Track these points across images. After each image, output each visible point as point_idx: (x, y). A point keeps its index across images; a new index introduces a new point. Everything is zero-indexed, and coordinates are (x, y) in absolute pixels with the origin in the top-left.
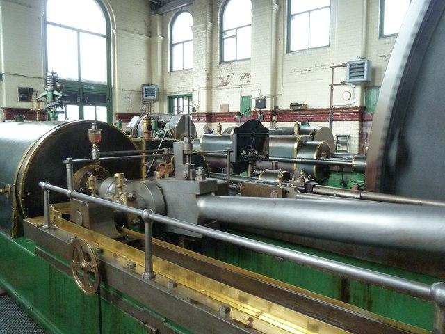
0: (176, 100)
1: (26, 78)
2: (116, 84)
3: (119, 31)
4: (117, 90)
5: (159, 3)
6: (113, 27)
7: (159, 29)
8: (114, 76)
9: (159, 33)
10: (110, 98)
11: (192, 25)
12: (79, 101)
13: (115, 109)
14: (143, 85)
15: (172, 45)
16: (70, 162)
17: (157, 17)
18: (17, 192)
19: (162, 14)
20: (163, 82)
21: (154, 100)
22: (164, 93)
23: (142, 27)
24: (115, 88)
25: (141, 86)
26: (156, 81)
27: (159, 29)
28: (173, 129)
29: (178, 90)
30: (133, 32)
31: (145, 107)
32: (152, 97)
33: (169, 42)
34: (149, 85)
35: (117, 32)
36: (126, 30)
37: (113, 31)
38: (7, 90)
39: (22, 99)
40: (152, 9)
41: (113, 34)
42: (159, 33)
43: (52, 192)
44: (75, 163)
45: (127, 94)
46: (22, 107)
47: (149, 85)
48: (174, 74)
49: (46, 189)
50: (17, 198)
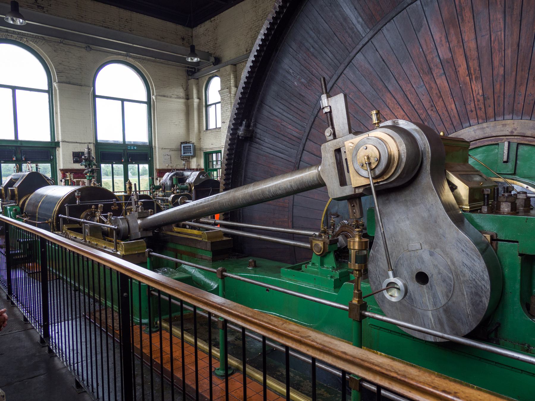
0: (214, 155)
1: (79, 144)
2: (156, 144)
3: (159, 97)
4: (157, 149)
5: (193, 70)
6: (153, 95)
7: (195, 92)
8: (155, 137)
9: (195, 95)
10: (152, 158)
11: (220, 89)
12: (123, 160)
13: (156, 166)
14: (182, 143)
15: (207, 106)
16: (67, 205)
17: (192, 82)
18: (53, 222)
19: (197, 79)
20: (199, 139)
21: (191, 156)
22: (200, 149)
23: (181, 92)
24: (155, 147)
25: (179, 144)
26: (193, 139)
27: (195, 92)
28: (192, 183)
29: (211, 147)
30: (171, 97)
31: (183, 162)
32: (189, 154)
33: (204, 104)
34: (186, 143)
35: (156, 99)
36: (164, 96)
37: (153, 97)
38: (63, 155)
39: (75, 162)
40: (189, 75)
41: (153, 99)
42: (195, 95)
43: (64, 219)
44: (69, 206)
45: (167, 152)
46: (75, 168)
47: (186, 143)
48: (208, 132)
49: (61, 217)
50: (53, 225)
